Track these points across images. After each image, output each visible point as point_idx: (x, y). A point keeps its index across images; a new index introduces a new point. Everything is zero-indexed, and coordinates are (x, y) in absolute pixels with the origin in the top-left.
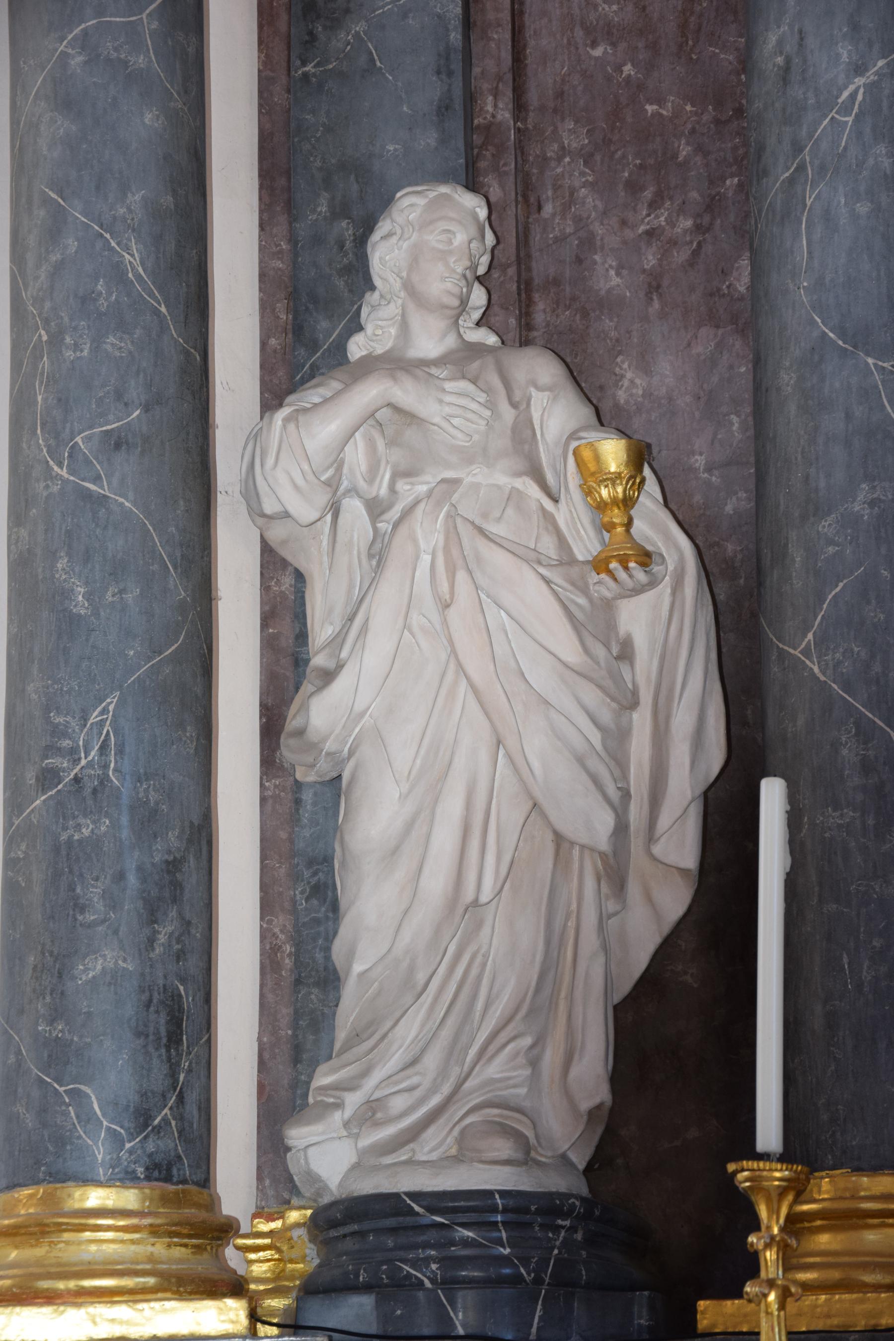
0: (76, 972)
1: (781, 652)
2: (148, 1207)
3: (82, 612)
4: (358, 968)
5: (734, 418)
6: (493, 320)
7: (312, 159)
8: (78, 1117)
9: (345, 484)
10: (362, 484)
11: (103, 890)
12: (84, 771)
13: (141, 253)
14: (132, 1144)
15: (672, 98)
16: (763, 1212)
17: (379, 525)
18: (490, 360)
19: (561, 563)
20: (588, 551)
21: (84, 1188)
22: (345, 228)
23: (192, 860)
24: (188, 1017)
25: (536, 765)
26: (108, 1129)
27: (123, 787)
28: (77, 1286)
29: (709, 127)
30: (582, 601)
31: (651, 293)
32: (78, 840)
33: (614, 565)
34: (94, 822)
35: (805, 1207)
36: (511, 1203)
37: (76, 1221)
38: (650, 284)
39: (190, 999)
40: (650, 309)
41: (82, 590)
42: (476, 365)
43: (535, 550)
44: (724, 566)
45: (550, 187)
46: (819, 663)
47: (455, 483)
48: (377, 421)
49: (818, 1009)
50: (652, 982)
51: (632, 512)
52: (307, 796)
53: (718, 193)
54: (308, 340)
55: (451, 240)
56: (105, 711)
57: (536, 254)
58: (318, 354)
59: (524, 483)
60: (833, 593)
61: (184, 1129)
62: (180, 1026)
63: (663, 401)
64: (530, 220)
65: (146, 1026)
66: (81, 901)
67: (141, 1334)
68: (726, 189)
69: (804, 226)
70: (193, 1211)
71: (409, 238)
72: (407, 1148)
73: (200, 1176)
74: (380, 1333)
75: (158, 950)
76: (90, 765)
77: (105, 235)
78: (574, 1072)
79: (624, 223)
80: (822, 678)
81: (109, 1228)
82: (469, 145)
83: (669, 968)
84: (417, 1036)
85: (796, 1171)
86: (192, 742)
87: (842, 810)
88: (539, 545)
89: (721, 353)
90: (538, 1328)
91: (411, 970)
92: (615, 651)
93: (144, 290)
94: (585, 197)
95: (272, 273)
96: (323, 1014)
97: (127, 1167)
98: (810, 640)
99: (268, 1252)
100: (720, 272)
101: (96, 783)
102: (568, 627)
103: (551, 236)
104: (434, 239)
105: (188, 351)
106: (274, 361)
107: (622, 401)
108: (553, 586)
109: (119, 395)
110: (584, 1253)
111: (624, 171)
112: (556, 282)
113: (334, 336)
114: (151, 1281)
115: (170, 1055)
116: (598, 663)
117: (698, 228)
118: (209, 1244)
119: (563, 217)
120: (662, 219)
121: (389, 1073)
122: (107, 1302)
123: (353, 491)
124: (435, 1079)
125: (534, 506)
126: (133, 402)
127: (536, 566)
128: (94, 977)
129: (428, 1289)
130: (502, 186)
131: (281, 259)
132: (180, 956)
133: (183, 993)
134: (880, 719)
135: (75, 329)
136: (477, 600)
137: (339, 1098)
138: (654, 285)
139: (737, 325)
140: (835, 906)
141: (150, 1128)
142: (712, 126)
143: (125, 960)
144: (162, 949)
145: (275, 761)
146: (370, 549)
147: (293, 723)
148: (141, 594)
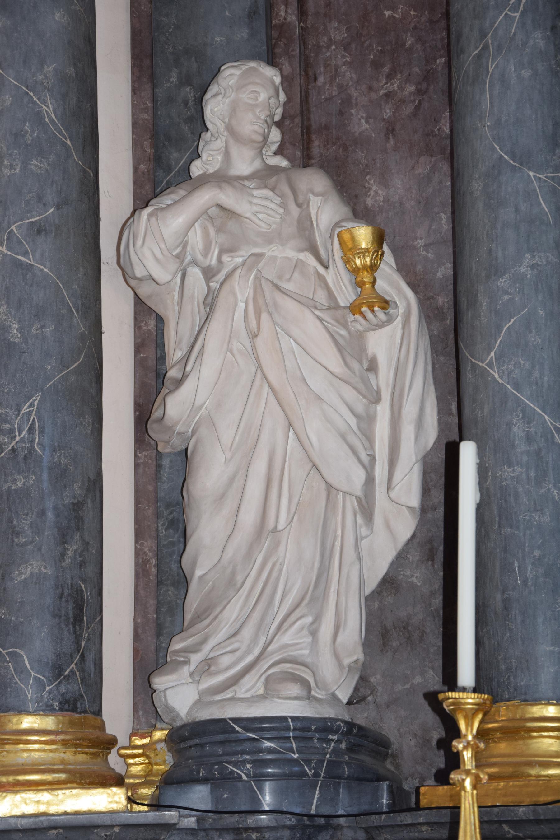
0: (13, 575)
1: (474, 365)
2: (61, 728)
3: (17, 341)
4: (198, 573)
5: (443, 216)
6: (285, 152)
7: (166, 47)
8: (15, 670)
9: (188, 258)
10: (200, 257)
11: (31, 522)
12: (18, 445)
13: (53, 105)
14: (51, 687)
15: (401, 6)
16: (462, 725)
17: (211, 284)
18: (283, 176)
19: (330, 308)
20: (348, 300)
21: (19, 716)
22: (188, 92)
23: (89, 502)
24: (87, 605)
25: (314, 439)
26: (35, 677)
27: (44, 454)
28: (14, 780)
29: (425, 25)
30: (343, 332)
31: (388, 134)
32: (14, 490)
33: (364, 309)
34: (25, 478)
35: (490, 726)
36: (299, 725)
37: (14, 737)
38: (387, 129)
39: (89, 593)
40: (388, 145)
41: (17, 326)
42: (274, 179)
43: (312, 299)
44: (436, 312)
45: (322, 65)
46: (498, 372)
47: (261, 255)
48: (209, 216)
49: (499, 597)
50: (389, 583)
51: (376, 274)
52: (166, 463)
53: (432, 68)
54: (164, 164)
55: (257, 97)
56: (32, 405)
57: (313, 109)
58: (172, 175)
59: (306, 256)
60: (508, 326)
61: (85, 677)
62: (82, 610)
63: (396, 205)
64: (310, 87)
65: (59, 610)
66: (17, 529)
67: (57, 811)
68: (437, 66)
69: (487, 85)
70: (91, 730)
71: (230, 96)
72: (231, 689)
73: (96, 708)
74: (214, 809)
75: (68, 561)
76: (22, 440)
77: (30, 93)
78: (339, 639)
79: (370, 88)
80: (501, 381)
81: (35, 742)
82: (269, 38)
83: (402, 573)
84: (237, 617)
85: (483, 699)
86: (89, 425)
87: (514, 467)
88: (315, 296)
89: (434, 173)
90: (317, 806)
91: (234, 573)
92: (365, 365)
93: (55, 129)
94: (345, 72)
95: (141, 122)
96: (177, 604)
97: (47, 702)
98: (492, 357)
99: (142, 758)
100: (433, 120)
101: (26, 452)
102: (335, 349)
103: (323, 97)
104: (245, 97)
105: (85, 170)
106: (143, 179)
107: (370, 205)
108: (324, 323)
109: (40, 199)
110: (346, 757)
111: (370, 55)
112: (327, 127)
113: (182, 162)
114: (63, 776)
115: (76, 629)
116: (354, 373)
117: (419, 92)
118: (101, 752)
119: (331, 85)
120: (396, 86)
121: (220, 641)
122: (34, 790)
123: (194, 262)
124: (249, 645)
125: (312, 271)
126: (49, 203)
127: (313, 310)
128: (25, 579)
129: (244, 781)
130: (291, 65)
131: (147, 113)
132: (82, 565)
133: (84, 589)
134: (538, 408)
135: (11, 155)
136: (275, 332)
137: (187, 658)
138: (390, 129)
139: (444, 154)
140: (509, 530)
141: (62, 677)
142: (428, 24)
143: (45, 568)
144: (70, 560)
145: (145, 440)
146: (205, 300)
147: (157, 414)
148: (55, 329)
